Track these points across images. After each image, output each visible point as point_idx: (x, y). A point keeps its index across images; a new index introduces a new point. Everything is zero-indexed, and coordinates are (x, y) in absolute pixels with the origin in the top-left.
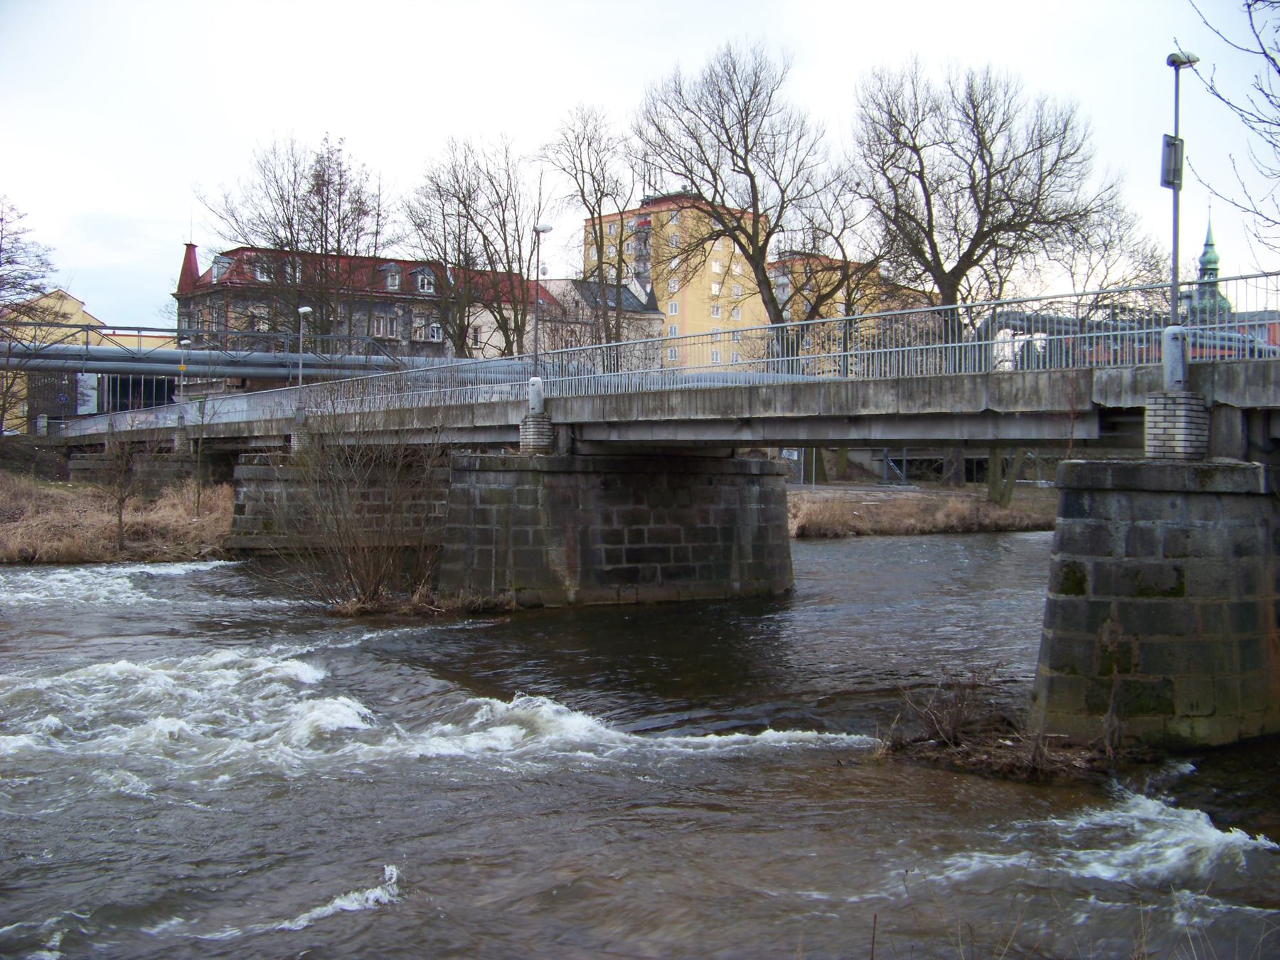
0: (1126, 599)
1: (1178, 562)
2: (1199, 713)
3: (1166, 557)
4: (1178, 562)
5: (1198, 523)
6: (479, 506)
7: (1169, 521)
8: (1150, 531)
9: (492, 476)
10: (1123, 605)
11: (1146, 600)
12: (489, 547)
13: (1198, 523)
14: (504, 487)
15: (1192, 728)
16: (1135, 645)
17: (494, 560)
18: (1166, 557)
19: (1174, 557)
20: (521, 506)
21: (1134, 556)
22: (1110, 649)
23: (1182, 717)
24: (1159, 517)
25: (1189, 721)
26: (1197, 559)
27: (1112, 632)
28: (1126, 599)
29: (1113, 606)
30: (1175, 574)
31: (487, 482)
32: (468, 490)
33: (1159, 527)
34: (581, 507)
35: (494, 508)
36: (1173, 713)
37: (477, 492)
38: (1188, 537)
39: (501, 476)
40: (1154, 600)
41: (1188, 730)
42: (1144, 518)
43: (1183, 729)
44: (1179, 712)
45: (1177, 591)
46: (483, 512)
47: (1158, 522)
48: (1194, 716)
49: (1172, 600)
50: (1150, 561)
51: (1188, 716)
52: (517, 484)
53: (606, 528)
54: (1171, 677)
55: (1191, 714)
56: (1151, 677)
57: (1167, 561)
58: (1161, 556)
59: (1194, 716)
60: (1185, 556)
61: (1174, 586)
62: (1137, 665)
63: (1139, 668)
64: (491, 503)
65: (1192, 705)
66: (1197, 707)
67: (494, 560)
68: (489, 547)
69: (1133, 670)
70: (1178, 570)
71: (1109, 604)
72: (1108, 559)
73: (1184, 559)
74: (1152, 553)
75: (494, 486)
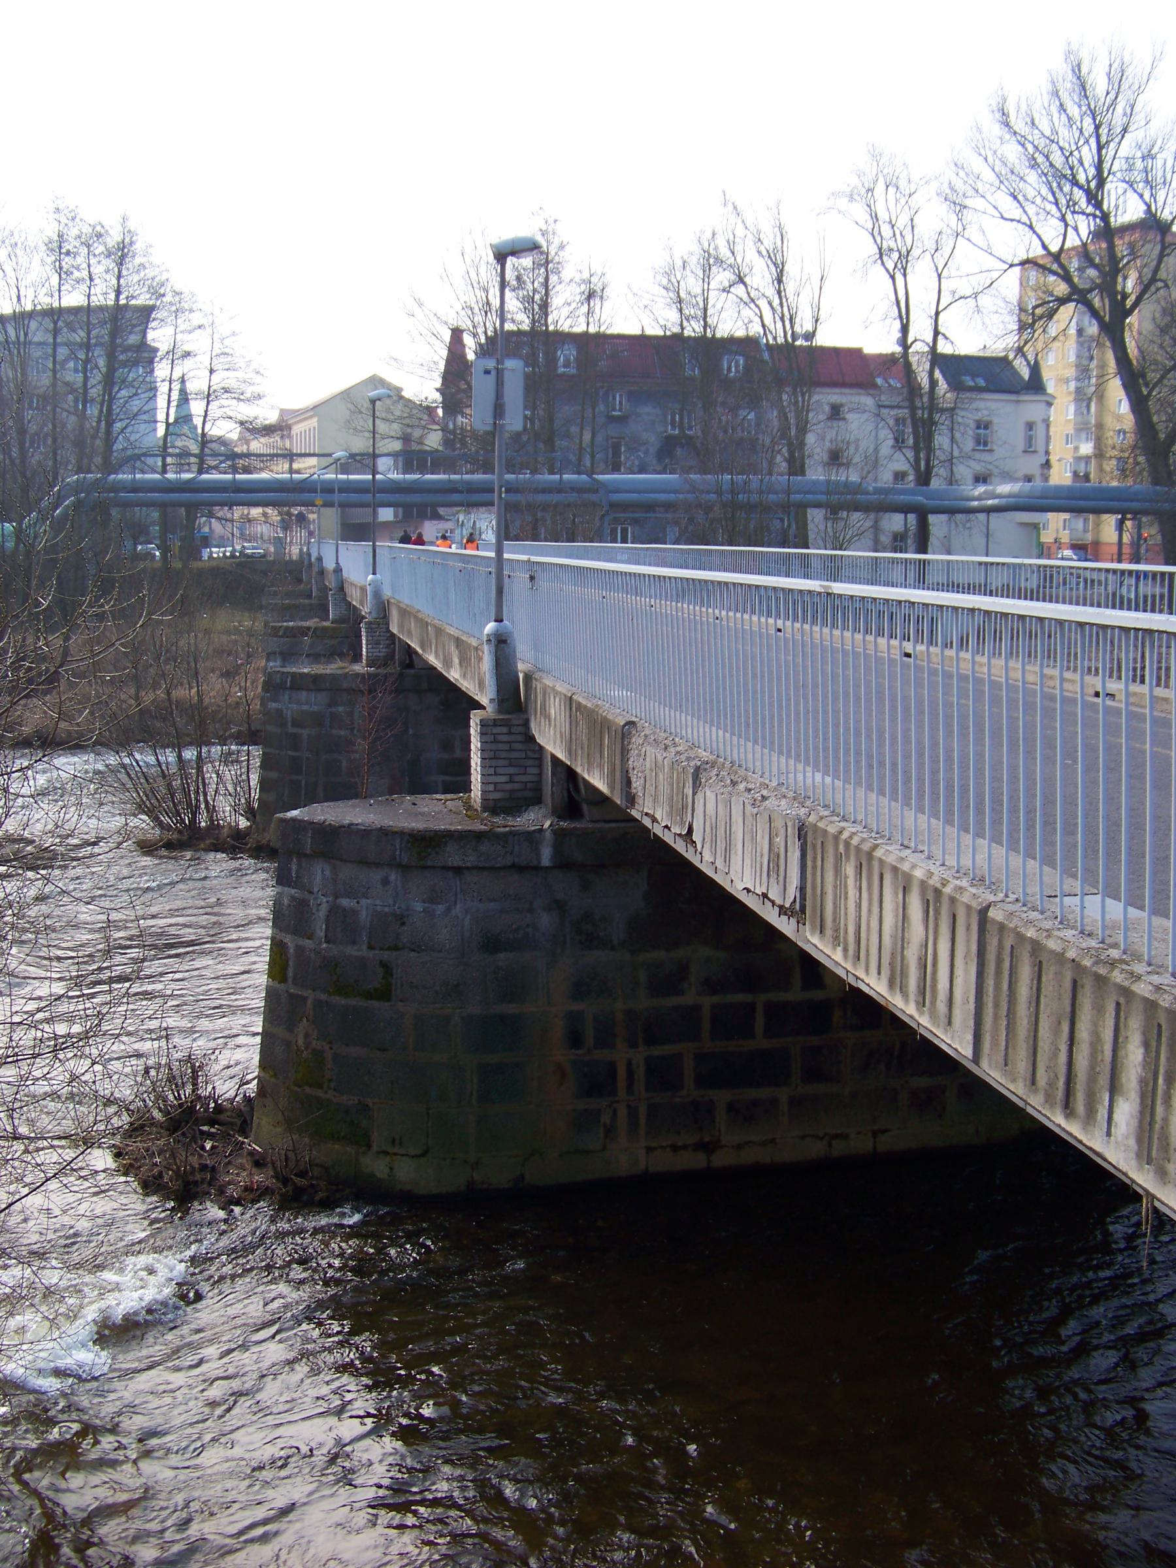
0: (323, 997)
1: (386, 955)
2: (402, 1151)
3: (371, 948)
4: (386, 955)
5: (418, 907)
6: (291, 730)
7: (378, 902)
8: (354, 912)
9: (304, 695)
10: (318, 1003)
11: (342, 1001)
12: (300, 778)
13: (418, 907)
14: (315, 708)
15: (391, 1169)
16: (329, 1055)
17: (303, 792)
18: (371, 948)
19: (381, 949)
20: (334, 732)
21: (334, 943)
22: (305, 1054)
23: (378, 1153)
24: (365, 896)
25: (388, 1158)
26: (412, 954)
27: (306, 1036)
28: (323, 997)
29: (309, 1002)
30: (380, 970)
31: (299, 703)
32: (281, 711)
33: (364, 908)
34: (411, 732)
35: (305, 732)
36: (369, 1146)
37: (289, 713)
38: (403, 924)
39: (313, 695)
40: (353, 1002)
41: (387, 1170)
42: (348, 896)
43: (378, 1167)
44: (375, 1148)
45: (384, 994)
46: (295, 736)
47: (364, 902)
48: (395, 1154)
49: (375, 1004)
50: (351, 951)
51: (386, 1153)
52: (330, 705)
53: (446, 756)
54: (369, 1101)
55: (391, 1150)
56: (345, 1097)
57: (371, 954)
58: (365, 947)
59: (395, 1154)
60: (396, 948)
61: (378, 986)
62: (330, 1080)
63: (332, 1085)
64: (302, 726)
65: (394, 1141)
66: (401, 1144)
67: (303, 792)
68: (300, 778)
69: (325, 1085)
70: (386, 967)
71: (305, 999)
72: (307, 943)
73: (395, 953)
74: (354, 942)
75: (305, 707)
